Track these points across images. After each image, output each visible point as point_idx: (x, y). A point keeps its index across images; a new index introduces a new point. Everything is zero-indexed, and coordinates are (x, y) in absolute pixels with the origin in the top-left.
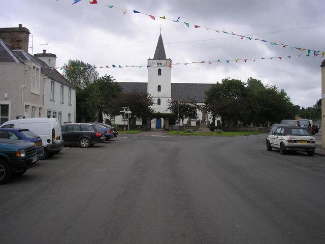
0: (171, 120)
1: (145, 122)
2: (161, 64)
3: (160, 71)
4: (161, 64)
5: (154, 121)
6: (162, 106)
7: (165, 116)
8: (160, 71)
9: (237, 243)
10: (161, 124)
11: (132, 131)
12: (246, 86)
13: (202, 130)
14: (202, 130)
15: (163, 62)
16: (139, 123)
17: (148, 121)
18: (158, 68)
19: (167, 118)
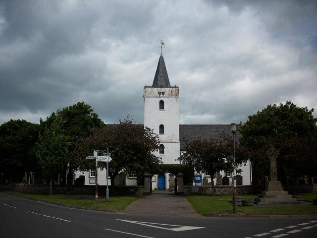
0: (183, 173)
1: (141, 182)
2: (163, 93)
3: (162, 103)
4: (163, 93)
5: (155, 178)
6: (171, 154)
7: (172, 169)
8: (162, 103)
9: (98, 237)
10: (164, 184)
11: (116, 199)
12: (21, 164)
13: (274, 196)
14: (274, 196)
15: (167, 90)
16: (130, 182)
17: (147, 179)
18: (159, 100)
19: (179, 174)
